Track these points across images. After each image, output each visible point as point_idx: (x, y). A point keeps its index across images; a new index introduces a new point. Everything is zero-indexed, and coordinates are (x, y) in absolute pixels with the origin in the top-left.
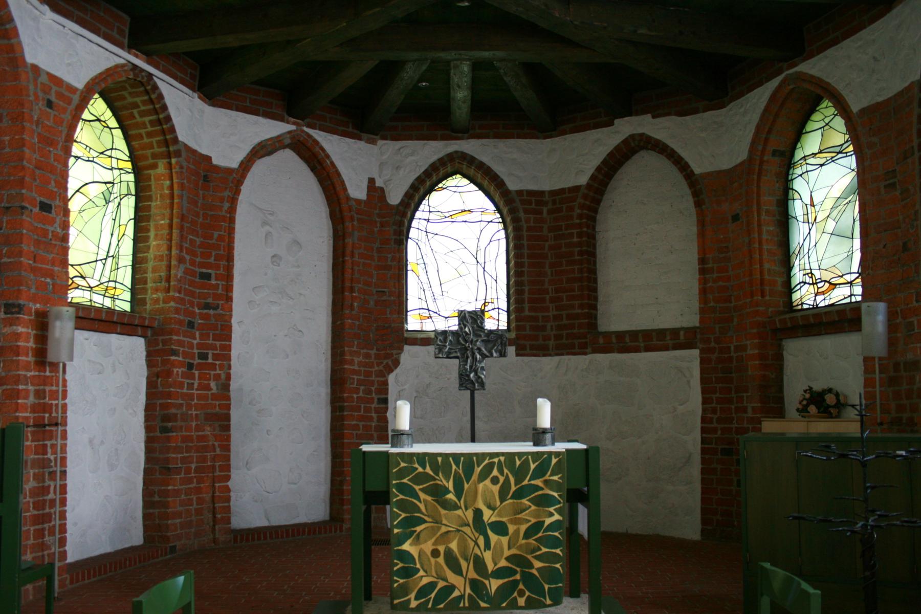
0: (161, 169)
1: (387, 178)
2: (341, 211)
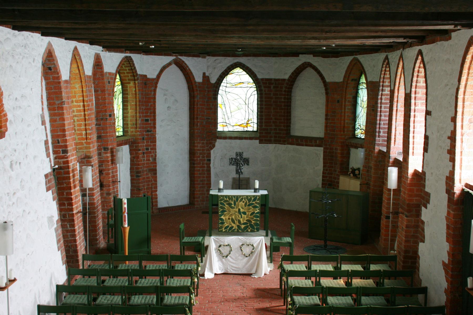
0: (132, 84)
1: (210, 72)
2: (193, 88)
